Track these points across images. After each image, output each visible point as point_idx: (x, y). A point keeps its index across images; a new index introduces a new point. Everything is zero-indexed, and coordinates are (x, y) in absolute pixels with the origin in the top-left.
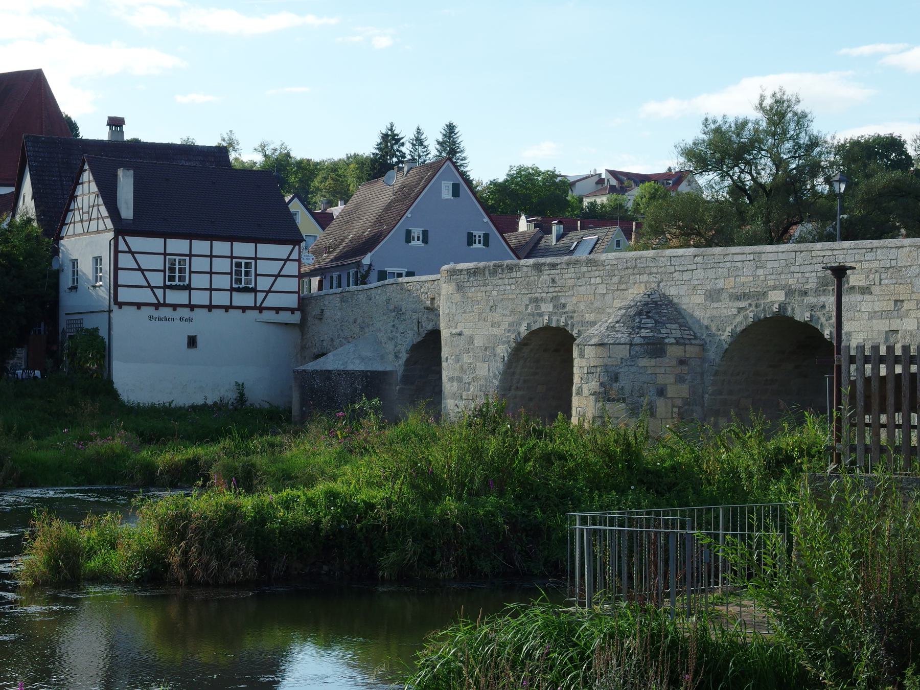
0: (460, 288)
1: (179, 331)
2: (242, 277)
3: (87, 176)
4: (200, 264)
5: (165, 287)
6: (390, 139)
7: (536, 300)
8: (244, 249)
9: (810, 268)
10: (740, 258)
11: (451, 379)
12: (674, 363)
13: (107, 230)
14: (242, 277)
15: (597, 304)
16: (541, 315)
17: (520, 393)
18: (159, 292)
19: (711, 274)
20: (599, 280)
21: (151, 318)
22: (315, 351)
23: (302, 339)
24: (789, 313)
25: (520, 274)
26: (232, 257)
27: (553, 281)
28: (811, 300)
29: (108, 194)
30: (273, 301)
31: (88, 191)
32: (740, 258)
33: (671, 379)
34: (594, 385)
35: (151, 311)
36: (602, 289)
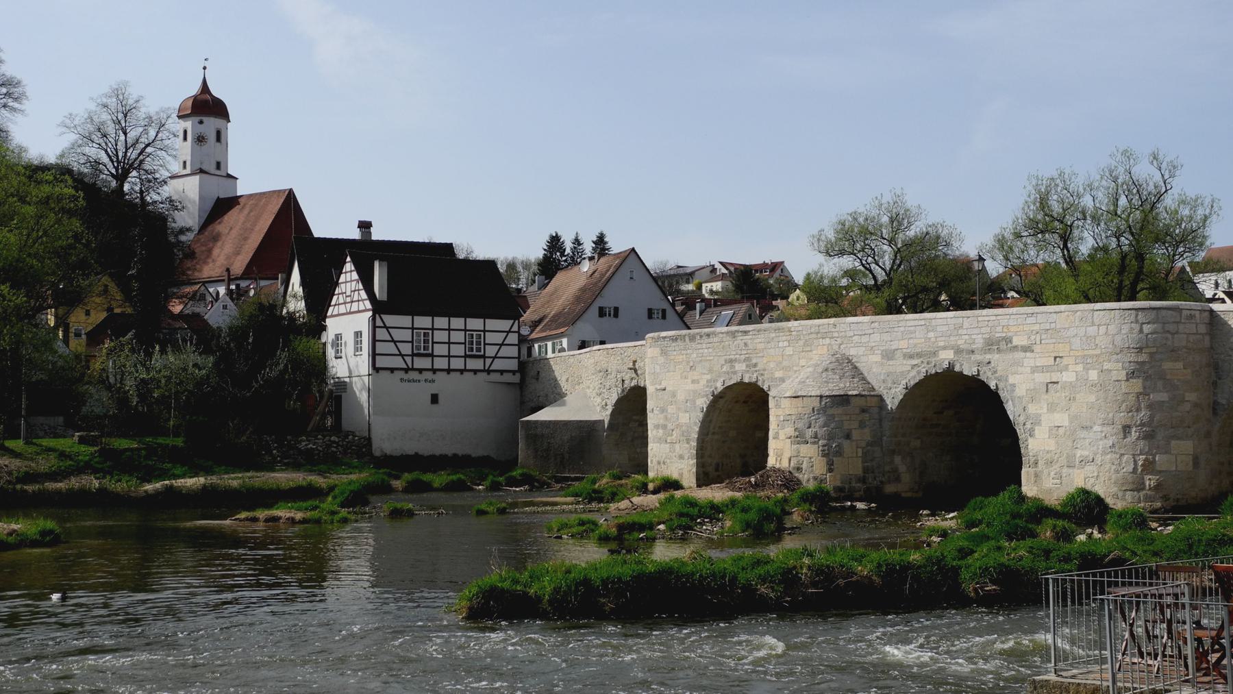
0: (664, 353)
1: (422, 391)
2: (474, 347)
3: (349, 266)
4: (490, 338)
5: (413, 355)
6: (555, 242)
7: (731, 361)
8: (475, 324)
9: (976, 331)
10: (912, 323)
11: (657, 427)
12: (857, 411)
13: (366, 310)
14: (474, 347)
15: (785, 363)
16: (735, 373)
17: (716, 437)
18: (408, 359)
19: (886, 337)
20: (786, 344)
21: (402, 380)
22: (532, 405)
23: (522, 396)
24: (957, 369)
25: (716, 339)
26: (465, 330)
27: (746, 344)
28: (978, 357)
29: (366, 279)
30: (498, 365)
31: (349, 277)
32: (912, 323)
33: (855, 425)
34: (790, 430)
35: (402, 374)
36: (789, 351)
